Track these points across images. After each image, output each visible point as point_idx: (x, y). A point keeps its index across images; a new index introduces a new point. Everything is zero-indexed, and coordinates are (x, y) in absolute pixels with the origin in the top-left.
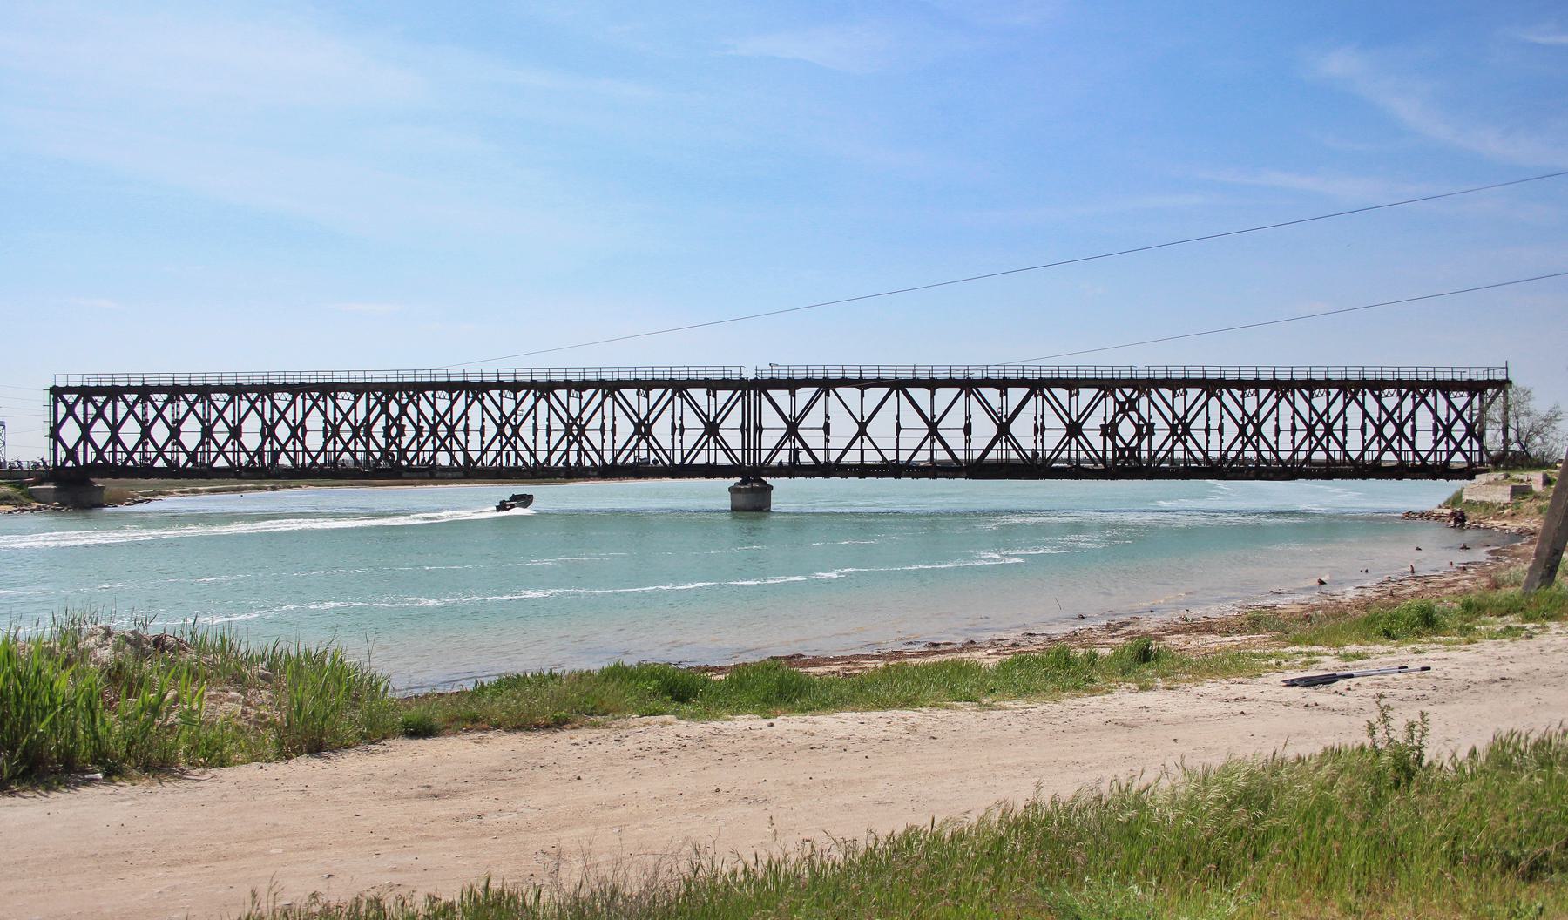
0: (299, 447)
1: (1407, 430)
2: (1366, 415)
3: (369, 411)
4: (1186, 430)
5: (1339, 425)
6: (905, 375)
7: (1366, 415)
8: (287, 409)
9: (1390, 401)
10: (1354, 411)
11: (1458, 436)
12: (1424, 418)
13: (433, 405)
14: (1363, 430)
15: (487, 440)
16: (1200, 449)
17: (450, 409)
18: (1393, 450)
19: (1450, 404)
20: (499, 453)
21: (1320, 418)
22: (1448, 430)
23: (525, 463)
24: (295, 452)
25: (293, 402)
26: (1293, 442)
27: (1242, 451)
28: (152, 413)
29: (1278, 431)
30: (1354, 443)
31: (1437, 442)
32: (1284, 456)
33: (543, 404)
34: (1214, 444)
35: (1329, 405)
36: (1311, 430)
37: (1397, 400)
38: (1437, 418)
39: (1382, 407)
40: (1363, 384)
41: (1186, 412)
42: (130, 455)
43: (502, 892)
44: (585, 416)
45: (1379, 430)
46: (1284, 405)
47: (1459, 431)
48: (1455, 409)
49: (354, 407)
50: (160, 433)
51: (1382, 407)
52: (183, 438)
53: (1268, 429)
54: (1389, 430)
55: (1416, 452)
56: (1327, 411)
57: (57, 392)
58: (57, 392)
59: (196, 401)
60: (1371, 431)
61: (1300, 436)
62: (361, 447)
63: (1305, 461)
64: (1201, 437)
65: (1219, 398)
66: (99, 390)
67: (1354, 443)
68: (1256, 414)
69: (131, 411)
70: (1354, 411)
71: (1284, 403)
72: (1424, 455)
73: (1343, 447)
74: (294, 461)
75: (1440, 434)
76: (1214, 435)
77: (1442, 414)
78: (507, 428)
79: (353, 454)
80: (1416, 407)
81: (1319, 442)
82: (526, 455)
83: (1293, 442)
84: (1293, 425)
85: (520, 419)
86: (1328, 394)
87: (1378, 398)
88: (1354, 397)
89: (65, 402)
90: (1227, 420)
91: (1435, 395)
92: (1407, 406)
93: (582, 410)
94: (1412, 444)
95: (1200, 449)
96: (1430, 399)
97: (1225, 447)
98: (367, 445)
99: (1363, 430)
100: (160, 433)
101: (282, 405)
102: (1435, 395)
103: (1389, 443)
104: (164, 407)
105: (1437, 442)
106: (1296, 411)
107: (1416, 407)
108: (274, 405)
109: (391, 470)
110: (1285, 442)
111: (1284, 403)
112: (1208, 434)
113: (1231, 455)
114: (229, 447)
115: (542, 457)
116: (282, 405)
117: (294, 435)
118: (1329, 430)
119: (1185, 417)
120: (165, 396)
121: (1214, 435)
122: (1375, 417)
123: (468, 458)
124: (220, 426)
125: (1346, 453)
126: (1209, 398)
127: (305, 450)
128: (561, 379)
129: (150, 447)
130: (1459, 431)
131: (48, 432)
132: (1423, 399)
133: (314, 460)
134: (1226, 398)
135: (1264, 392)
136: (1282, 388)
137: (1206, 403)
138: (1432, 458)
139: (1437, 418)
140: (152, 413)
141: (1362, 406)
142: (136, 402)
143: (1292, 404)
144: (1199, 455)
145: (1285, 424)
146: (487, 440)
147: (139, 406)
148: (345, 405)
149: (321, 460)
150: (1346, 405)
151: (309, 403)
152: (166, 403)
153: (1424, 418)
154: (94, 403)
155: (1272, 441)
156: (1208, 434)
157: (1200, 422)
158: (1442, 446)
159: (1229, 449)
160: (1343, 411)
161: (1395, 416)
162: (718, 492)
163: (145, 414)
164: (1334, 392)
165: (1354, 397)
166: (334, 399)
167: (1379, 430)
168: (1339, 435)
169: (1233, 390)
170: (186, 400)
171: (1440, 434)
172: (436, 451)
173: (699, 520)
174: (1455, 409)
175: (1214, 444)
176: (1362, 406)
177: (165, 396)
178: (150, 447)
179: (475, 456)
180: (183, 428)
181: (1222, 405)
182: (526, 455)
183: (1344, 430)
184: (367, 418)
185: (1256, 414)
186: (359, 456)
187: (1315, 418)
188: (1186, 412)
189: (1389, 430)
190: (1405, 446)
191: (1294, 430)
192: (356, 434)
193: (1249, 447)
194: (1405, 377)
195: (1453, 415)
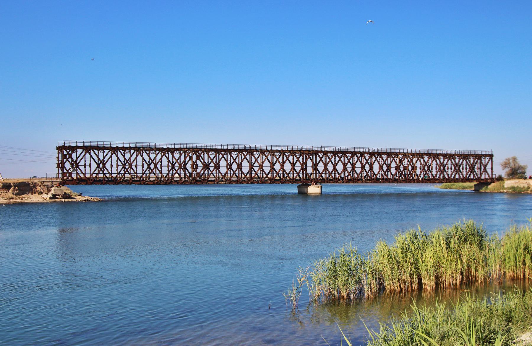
3: (185, 158)
4: (77, 166)
8: (214, 158)
9: (177, 156)
10: (139, 158)
11: (177, 168)
12: (165, 161)
13: (124, 156)
14: (143, 166)
15: (145, 169)
16: (82, 173)
25: (215, 156)
27: (97, 174)
28: (347, 161)
30: (140, 171)
31: (169, 172)
32: (88, 176)
34: (88, 171)
35: (131, 156)
37: (155, 155)
38: (169, 161)
39: (150, 158)
40: (144, 149)
41: (77, 158)
43: (347, 316)
44: (106, 159)
46: (88, 155)
48: (211, 158)
50: (277, 167)
52: (264, 168)
53: (108, 165)
54: (152, 166)
56: (130, 159)
57: (60, 149)
58: (60, 149)
59: (247, 155)
60: (146, 166)
62: (182, 172)
63: (96, 177)
64: (82, 168)
65: (90, 154)
67: (140, 171)
68: (103, 160)
70: (139, 158)
71: (114, 155)
76: (88, 168)
77: (206, 160)
78: (101, 165)
79: (179, 175)
83: (117, 170)
85: (132, 161)
86: (104, 152)
87: (148, 155)
88: (164, 155)
89: (338, 156)
90: (93, 162)
92: (159, 157)
93: (104, 157)
95: (82, 173)
97: (92, 172)
98: (184, 171)
100: (277, 167)
101: (235, 157)
105: (169, 172)
106: (118, 158)
107: (162, 157)
108: (209, 157)
109: (199, 180)
111: (114, 155)
112: (85, 167)
113: (94, 176)
116: (235, 157)
118: (130, 165)
119: (76, 160)
120: (332, 154)
121: (88, 168)
122: (147, 161)
123: (463, 176)
124: (367, 165)
126: (86, 153)
131: (56, 166)
134: (92, 153)
135: (106, 151)
136: (114, 150)
137: (85, 156)
139: (169, 161)
140: (254, 160)
141: (142, 156)
142: (342, 156)
143: (117, 156)
144: (108, 176)
145: (114, 164)
146: (145, 169)
147: (343, 158)
148: (212, 156)
150: (137, 156)
151: (221, 156)
152: (323, 156)
153: (165, 161)
154: (296, 156)
156: (85, 167)
157: (82, 163)
159: (93, 173)
160: (136, 159)
162: (293, 189)
163: (344, 161)
166: (173, 154)
169: (95, 150)
171: (170, 168)
173: (292, 196)
174: (211, 158)
175: (88, 171)
176: (142, 156)
180: (285, 165)
181: (91, 156)
184: (184, 161)
185: (103, 160)
186: (182, 176)
188: (77, 158)
189: (152, 166)
190: (158, 172)
192: (180, 168)
193: (101, 172)
195: (210, 161)
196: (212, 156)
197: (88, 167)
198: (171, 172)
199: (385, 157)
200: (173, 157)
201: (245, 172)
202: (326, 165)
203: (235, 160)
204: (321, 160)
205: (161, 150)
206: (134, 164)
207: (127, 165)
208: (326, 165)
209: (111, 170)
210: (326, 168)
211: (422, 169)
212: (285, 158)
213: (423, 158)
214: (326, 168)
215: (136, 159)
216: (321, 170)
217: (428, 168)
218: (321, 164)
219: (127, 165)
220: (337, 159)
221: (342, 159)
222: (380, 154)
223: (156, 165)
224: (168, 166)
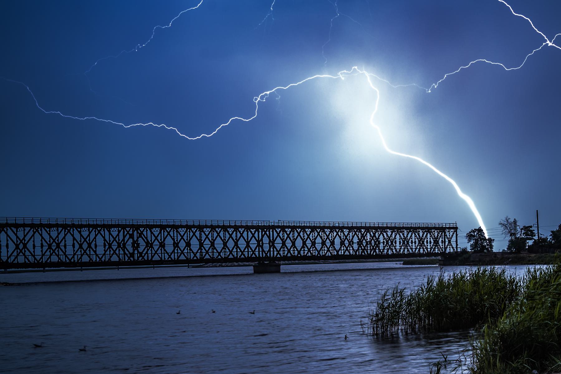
1: (93, 246)
2: (74, 239)
3: (124, 237)
5: (63, 244)
6: (190, 223)
7: (74, 239)
9: (85, 233)
10: (69, 238)
12: (100, 241)
14: (74, 246)
15: (76, 249)
17: (89, 235)
18: (87, 254)
20: (16, 257)
21: (21, 241)
23: (74, 261)
24: (273, 251)
26: (42, 251)
29: (34, 246)
31: (106, 251)
35: (59, 234)
36: (50, 246)
37: (88, 233)
38: (105, 240)
39: (81, 236)
42: (219, 253)
45: (81, 246)
47: (115, 246)
49: (118, 235)
51: (81, 236)
53: (30, 246)
54: (85, 246)
55: (97, 255)
60: (77, 246)
61: (45, 249)
62: (121, 252)
66: (253, 227)
72: (100, 256)
75: (107, 247)
77: (107, 238)
80: (96, 235)
81: (21, 251)
82: (30, 258)
84: (42, 244)
86: (58, 230)
87: (80, 232)
90: (10, 242)
91: (104, 230)
94: (95, 252)
96: (102, 232)
99: (74, 246)
101: (156, 234)
102: (104, 230)
103: (85, 251)
104: (290, 233)
105: (106, 251)
106: (42, 238)
107: (96, 235)
110: (38, 252)
114: (186, 251)
115: (38, 258)
116: (156, 234)
118: (58, 246)
120: (290, 230)
124: (288, 241)
128: (22, 222)
129: (203, 251)
130: (115, 246)
132: (69, 231)
133: (100, 259)
135: (27, 229)
138: (104, 258)
139: (105, 240)
141: (73, 235)
145: (38, 244)
147: (222, 232)
148: (115, 234)
149: (103, 259)
152: (290, 232)
155: (32, 250)
158: (108, 252)
160: (64, 238)
161: (87, 240)
164: (60, 229)
167: (81, 246)
168: (63, 248)
169: (13, 228)
170: (317, 231)
171: (107, 247)
177: (290, 230)
178: (203, 251)
179: (38, 258)
181: (8, 235)
182: (30, 258)
183: (65, 246)
184: (123, 240)
187: (52, 241)
189: (85, 246)
190: (92, 252)
191: (42, 246)
192: (119, 246)
194: (91, 223)
201: (337, 248)
207: (21, 246)
209: (34, 252)
219: (55, 246)
224: (105, 246)
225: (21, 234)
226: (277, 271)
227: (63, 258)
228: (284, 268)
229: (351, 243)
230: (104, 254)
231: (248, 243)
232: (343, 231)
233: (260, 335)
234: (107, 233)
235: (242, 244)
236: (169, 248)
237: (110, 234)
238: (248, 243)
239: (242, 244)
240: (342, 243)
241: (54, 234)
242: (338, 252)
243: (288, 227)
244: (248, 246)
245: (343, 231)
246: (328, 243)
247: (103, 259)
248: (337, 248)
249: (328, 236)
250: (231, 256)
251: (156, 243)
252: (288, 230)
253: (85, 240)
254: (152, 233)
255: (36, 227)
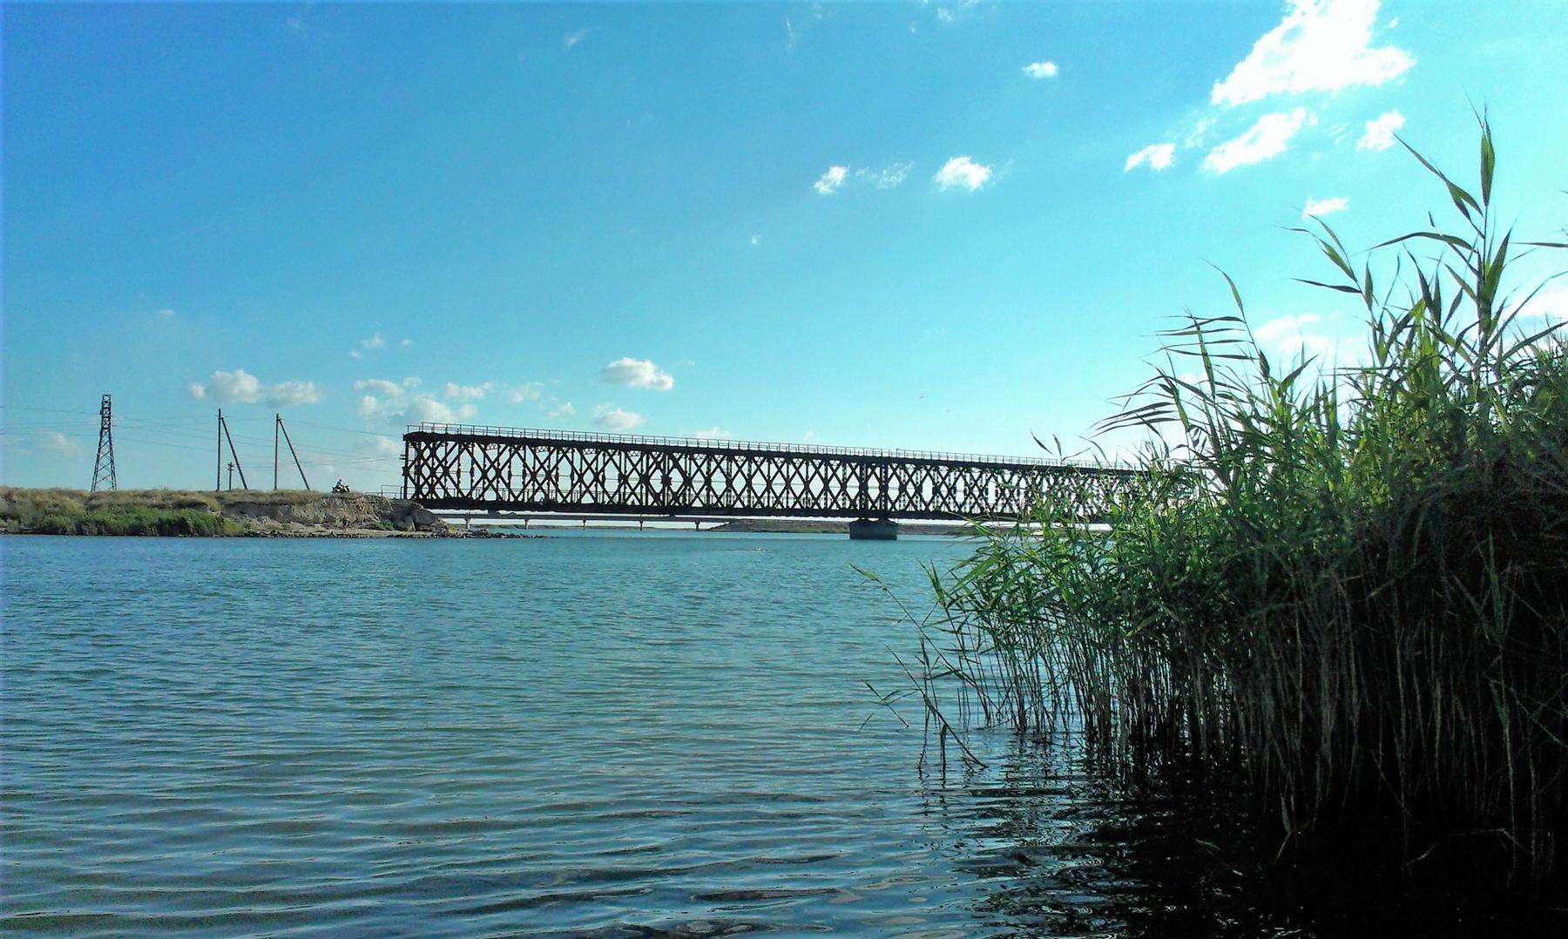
0: (600, 489)
2: (474, 461)
7: (474, 461)
11: (540, 480)
12: (565, 468)
19: (536, 457)
22: (534, 475)
28: (830, 473)
33: (465, 456)
35: (500, 454)
38: (525, 465)
55: (511, 492)
57: (412, 439)
58: (412, 439)
60: (478, 474)
69: (817, 471)
73: (457, 486)
74: (595, 499)
77: (577, 465)
87: (484, 450)
88: (466, 448)
94: (508, 485)
100: (739, 483)
101: (635, 460)
105: (573, 486)
116: (635, 460)
117: (596, 479)
124: (910, 485)
125: (459, 491)
127: (605, 491)
132: (565, 455)
139: (525, 465)
146: (476, 479)
148: (590, 458)
153: (565, 468)
160: (458, 458)
165: (466, 448)
172: (485, 490)
189: (492, 474)
190: (502, 485)
195: (585, 466)
196: (590, 458)
197: (464, 475)
198: (530, 487)
199: (944, 470)
200: (536, 457)
201: (927, 499)
202: (788, 481)
203: (635, 467)
204: (817, 471)
205: (510, 442)
206: (454, 468)
208: (788, 481)
210: (788, 487)
211: (1000, 495)
212: (754, 467)
213: (969, 471)
214: (788, 487)
215: (458, 458)
216: (778, 489)
217: (1003, 493)
218: (779, 480)
220: (713, 465)
221: (822, 470)
222: (935, 464)
223: (498, 472)
224: (557, 476)
225: (493, 454)
226: (893, 538)
227: (453, 493)
228: (899, 537)
229: (952, 490)
230: (571, 492)
231: (769, 482)
232: (937, 470)
233: (202, 771)
234: (577, 455)
235: (759, 483)
236: (612, 485)
237: (583, 457)
238: (769, 482)
239: (759, 483)
240: (936, 490)
241: (492, 453)
242: (927, 505)
243: (836, 457)
244: (769, 488)
245: (937, 470)
246: (911, 490)
247: (616, 499)
248: (927, 499)
249: (910, 477)
250: (738, 505)
251: (635, 475)
252: (834, 463)
253: (542, 465)
254: (583, 457)
255: (515, 444)
